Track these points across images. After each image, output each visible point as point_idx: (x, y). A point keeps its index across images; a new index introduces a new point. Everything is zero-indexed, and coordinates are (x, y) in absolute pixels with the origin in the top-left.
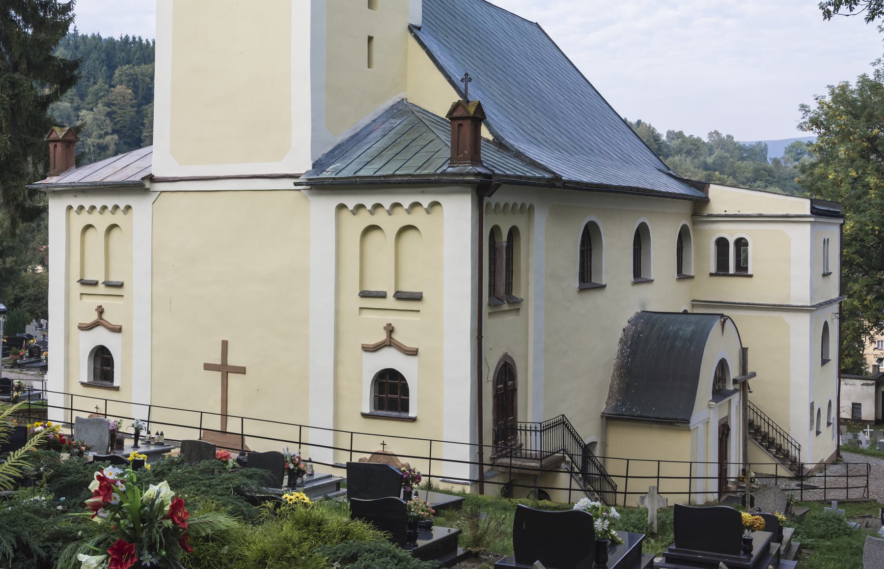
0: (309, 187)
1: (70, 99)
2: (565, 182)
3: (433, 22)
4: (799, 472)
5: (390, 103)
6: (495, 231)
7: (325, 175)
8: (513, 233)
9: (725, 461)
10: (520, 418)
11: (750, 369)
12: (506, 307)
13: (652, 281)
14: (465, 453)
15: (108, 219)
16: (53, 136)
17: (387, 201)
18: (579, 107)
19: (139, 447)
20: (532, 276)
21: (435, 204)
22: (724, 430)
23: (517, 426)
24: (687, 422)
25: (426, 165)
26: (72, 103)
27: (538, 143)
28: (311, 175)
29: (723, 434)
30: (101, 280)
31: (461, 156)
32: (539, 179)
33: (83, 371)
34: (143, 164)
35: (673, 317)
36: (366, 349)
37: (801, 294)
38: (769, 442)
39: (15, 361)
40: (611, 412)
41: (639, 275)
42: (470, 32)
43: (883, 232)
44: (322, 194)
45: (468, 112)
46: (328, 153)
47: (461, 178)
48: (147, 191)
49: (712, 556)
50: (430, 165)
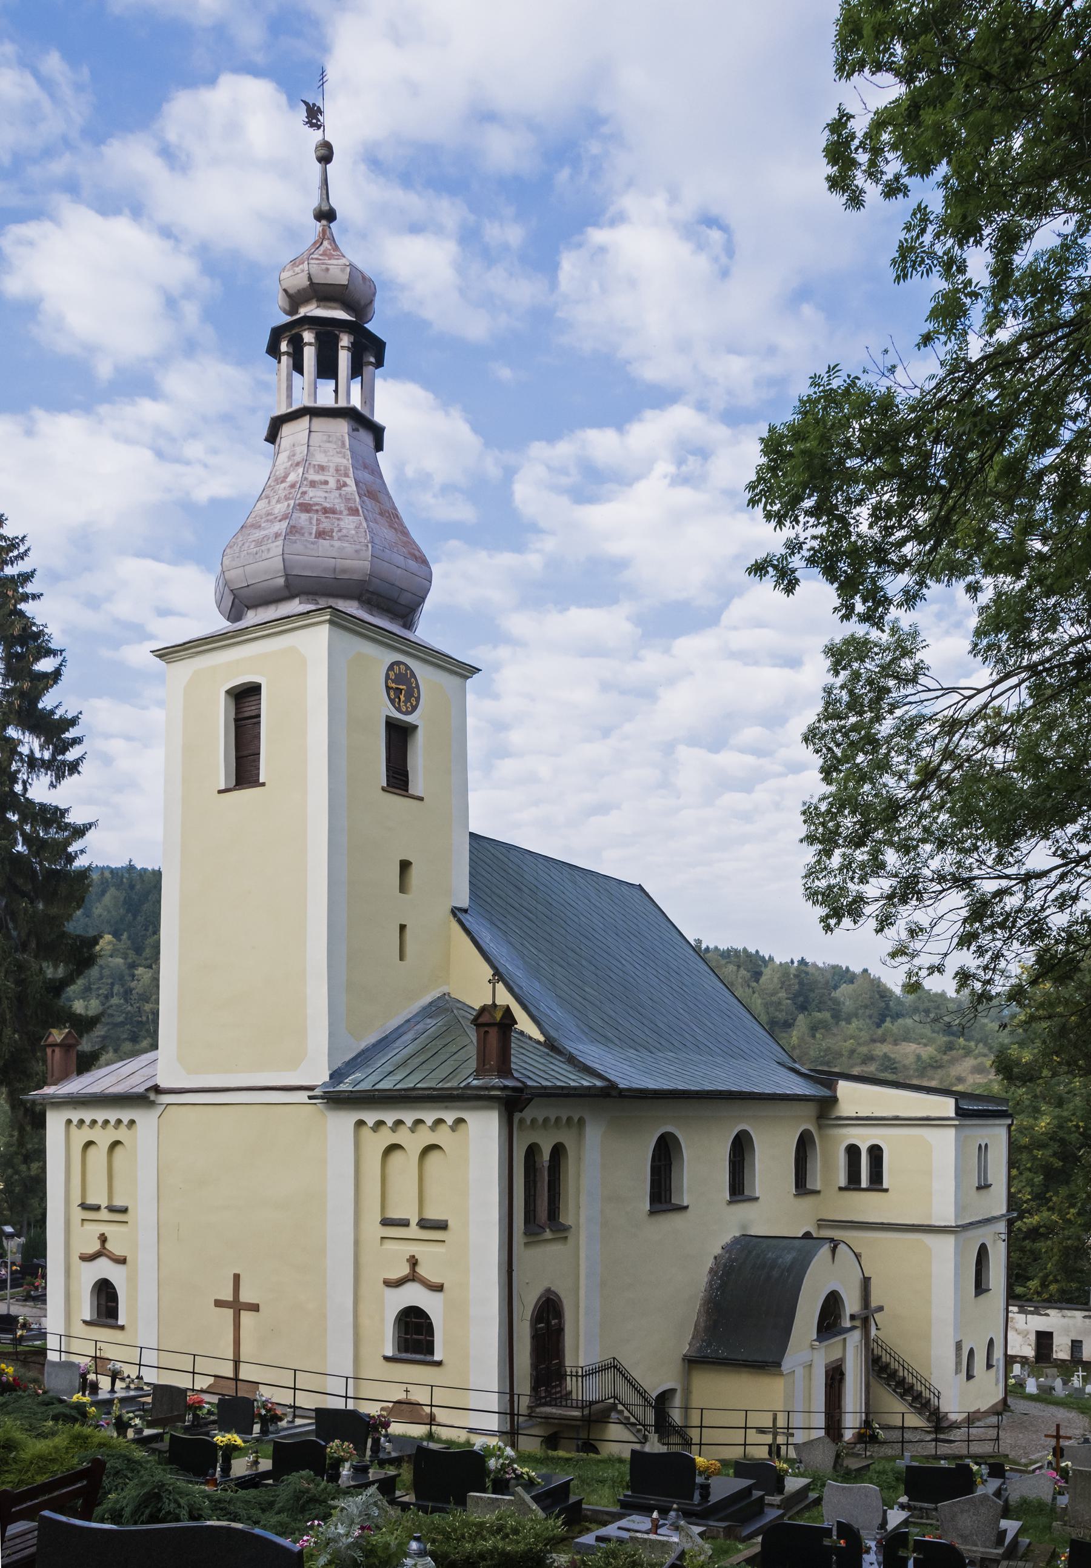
0: (325, 1101)
1: (123, 954)
2: (622, 1090)
3: (489, 900)
4: (938, 1423)
5: (427, 999)
6: (532, 1152)
7: (342, 1087)
8: (558, 1151)
9: (837, 1411)
10: (569, 1361)
11: (874, 1303)
12: (548, 1234)
13: (757, 1199)
14: (493, 1402)
15: (111, 1135)
16: (50, 1040)
17: (409, 1117)
18: (680, 990)
19: (115, 1392)
20: (583, 1199)
21: (460, 1121)
22: (835, 1377)
23: (566, 1372)
24: (778, 1365)
25: (451, 1076)
26: (125, 958)
27: (604, 1040)
28: (327, 1088)
29: (833, 1378)
30: (104, 1204)
31: (487, 1067)
32: (589, 1088)
33: (85, 1309)
34: (147, 1071)
35: (774, 1242)
36: (389, 1284)
37: (944, 1213)
38: (904, 1389)
39: (28, 1292)
40: (694, 1355)
41: (738, 1189)
42: (539, 907)
43: (1090, 1129)
44: (340, 1109)
45: (495, 1018)
46: (349, 1062)
47: (486, 1093)
48: (152, 1104)
49: (663, 1501)
50: (454, 1077)
